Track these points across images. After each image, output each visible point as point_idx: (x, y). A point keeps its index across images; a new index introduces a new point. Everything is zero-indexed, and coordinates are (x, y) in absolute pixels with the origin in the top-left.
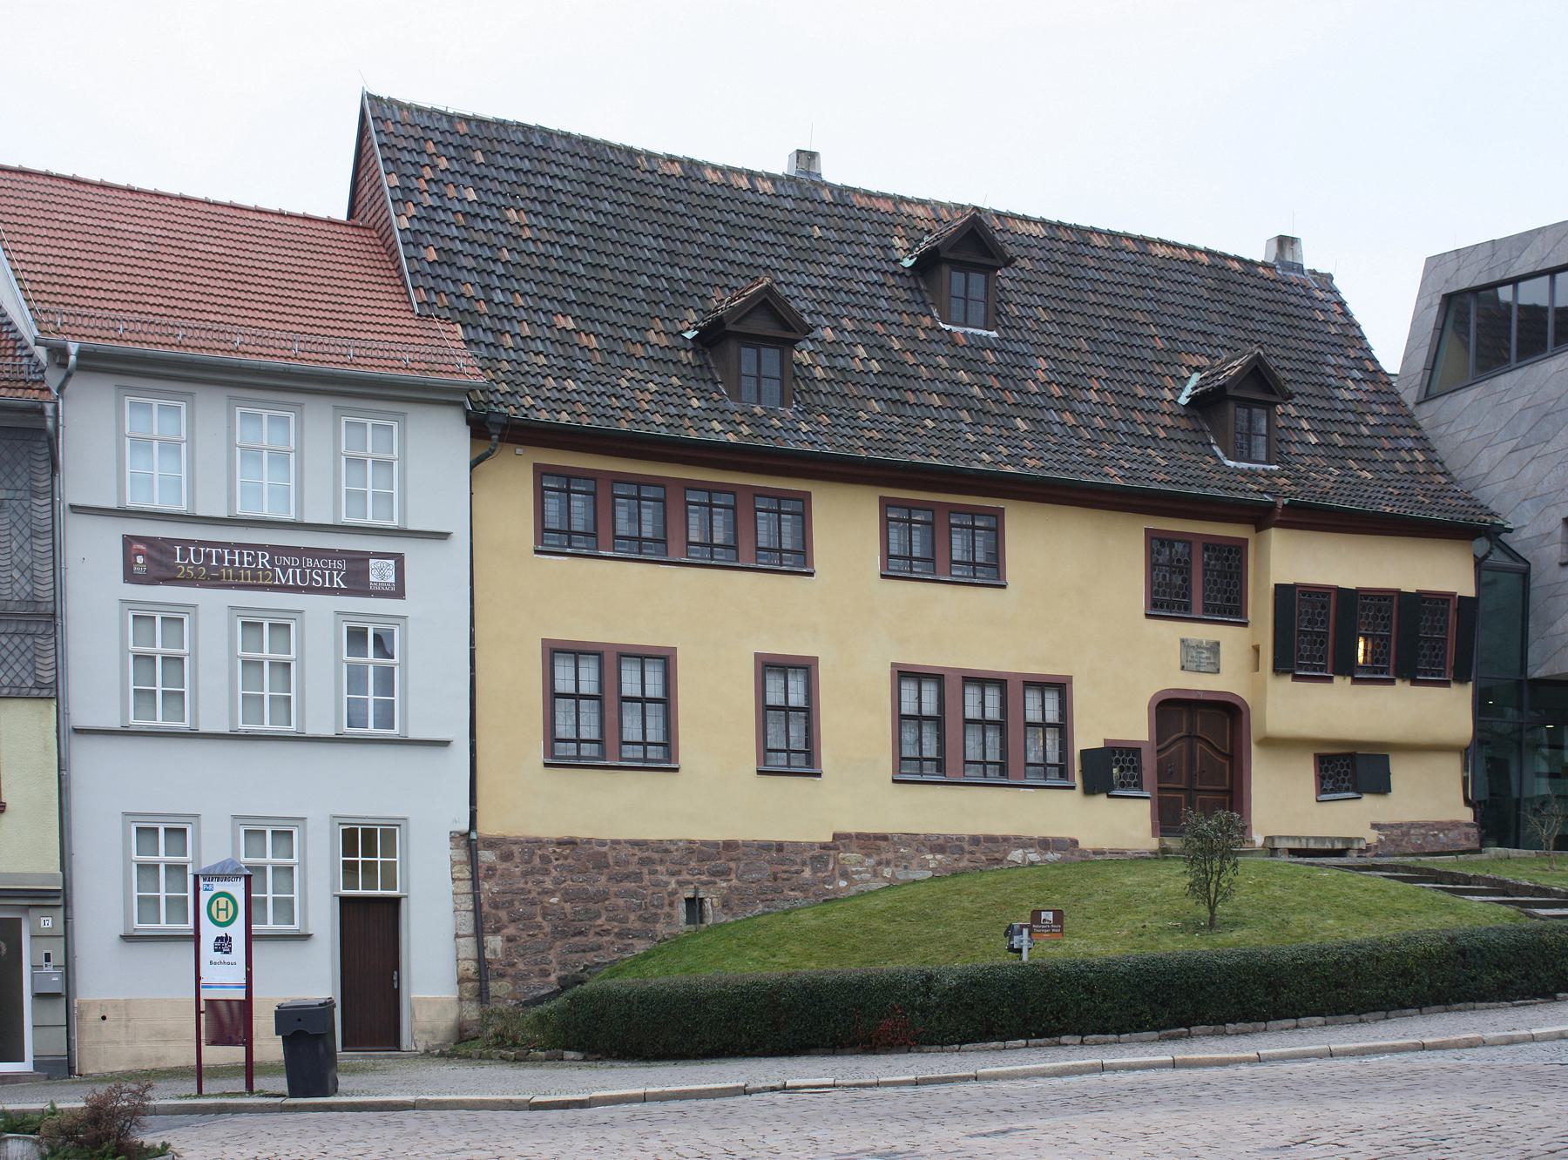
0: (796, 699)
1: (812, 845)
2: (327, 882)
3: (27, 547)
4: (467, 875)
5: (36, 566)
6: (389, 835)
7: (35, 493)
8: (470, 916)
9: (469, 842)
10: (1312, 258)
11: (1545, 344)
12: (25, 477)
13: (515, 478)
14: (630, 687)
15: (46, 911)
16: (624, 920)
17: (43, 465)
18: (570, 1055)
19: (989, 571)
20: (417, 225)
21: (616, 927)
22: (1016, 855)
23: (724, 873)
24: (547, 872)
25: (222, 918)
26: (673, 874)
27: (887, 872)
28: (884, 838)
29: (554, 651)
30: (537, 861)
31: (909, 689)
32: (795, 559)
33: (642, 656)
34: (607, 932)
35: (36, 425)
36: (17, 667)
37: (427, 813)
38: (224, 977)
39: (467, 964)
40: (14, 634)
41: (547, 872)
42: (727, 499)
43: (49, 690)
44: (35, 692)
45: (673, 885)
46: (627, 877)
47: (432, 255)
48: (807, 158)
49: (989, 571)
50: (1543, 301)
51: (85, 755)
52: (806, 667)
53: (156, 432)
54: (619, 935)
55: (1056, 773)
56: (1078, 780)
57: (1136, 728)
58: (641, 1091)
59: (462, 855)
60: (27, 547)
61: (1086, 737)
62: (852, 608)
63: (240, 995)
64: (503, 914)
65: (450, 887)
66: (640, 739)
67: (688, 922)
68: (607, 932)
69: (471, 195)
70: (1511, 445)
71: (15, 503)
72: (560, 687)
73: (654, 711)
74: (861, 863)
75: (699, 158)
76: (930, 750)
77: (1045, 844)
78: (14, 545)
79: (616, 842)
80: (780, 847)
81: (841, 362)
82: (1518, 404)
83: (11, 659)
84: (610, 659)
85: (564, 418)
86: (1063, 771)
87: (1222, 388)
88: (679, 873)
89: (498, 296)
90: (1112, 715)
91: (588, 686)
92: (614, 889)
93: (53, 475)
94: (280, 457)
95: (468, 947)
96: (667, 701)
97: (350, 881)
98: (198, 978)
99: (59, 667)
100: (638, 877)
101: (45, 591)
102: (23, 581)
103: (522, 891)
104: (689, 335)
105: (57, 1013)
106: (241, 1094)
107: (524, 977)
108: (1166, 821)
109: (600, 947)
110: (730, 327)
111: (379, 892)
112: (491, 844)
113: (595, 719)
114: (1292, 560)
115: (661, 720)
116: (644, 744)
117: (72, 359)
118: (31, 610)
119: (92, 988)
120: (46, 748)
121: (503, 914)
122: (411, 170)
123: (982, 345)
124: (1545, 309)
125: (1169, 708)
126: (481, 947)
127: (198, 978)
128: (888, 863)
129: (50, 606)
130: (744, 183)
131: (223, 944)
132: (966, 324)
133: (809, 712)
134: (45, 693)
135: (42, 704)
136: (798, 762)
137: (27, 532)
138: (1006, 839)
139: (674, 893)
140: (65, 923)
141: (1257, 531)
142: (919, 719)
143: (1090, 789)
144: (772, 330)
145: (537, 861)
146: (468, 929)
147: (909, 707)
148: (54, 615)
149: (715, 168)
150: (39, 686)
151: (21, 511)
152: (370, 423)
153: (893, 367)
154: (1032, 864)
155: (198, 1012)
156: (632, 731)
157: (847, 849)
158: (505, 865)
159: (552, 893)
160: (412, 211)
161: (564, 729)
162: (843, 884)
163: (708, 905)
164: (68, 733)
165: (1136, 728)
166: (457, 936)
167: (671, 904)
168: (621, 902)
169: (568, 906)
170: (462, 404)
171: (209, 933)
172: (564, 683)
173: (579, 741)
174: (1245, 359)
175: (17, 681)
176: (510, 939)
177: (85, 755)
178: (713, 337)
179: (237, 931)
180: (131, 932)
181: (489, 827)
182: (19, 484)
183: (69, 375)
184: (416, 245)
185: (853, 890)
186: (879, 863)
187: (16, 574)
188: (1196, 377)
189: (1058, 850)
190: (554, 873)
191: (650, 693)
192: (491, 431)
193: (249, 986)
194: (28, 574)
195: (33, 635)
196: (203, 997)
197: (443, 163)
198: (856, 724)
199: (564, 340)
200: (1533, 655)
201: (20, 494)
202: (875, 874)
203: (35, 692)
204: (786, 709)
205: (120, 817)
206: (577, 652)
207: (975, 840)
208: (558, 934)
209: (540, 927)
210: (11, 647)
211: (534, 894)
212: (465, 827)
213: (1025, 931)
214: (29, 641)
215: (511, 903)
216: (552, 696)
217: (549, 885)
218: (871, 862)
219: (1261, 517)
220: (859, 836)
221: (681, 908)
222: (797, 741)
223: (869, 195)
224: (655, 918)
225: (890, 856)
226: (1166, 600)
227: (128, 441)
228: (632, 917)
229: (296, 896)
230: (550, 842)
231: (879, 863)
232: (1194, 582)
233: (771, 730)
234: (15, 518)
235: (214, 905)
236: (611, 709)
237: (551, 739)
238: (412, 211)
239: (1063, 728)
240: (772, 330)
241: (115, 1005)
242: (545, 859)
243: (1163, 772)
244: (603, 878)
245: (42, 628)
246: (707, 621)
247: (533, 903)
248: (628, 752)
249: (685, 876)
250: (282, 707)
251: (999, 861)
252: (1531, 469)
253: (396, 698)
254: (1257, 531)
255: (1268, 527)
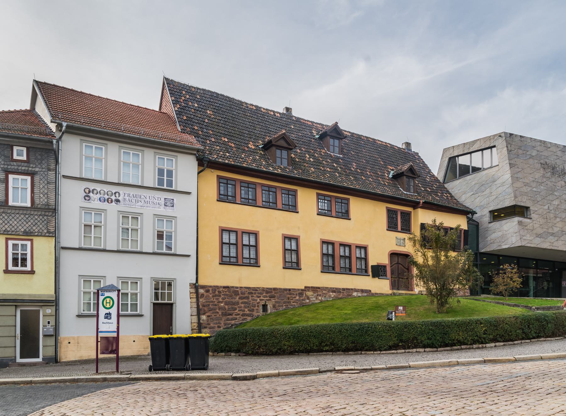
0: (294, 247)
1: (299, 290)
2: (149, 298)
3: (46, 187)
4: (195, 296)
5: (49, 193)
6: (170, 285)
7: (49, 170)
8: (195, 309)
9: (196, 287)
10: (414, 149)
11: (469, 173)
12: (46, 165)
13: (211, 177)
14: (246, 242)
15: (49, 307)
16: (244, 311)
17: (53, 161)
18: (233, 354)
19: (345, 215)
20: (180, 110)
21: (241, 313)
22: (355, 294)
23: (273, 297)
24: (220, 296)
25: (108, 306)
26: (259, 297)
27: (320, 298)
28: (319, 288)
29: (223, 230)
30: (217, 293)
31: (325, 246)
32: (293, 208)
33: (249, 233)
34: (239, 314)
35: (50, 148)
36: (41, 226)
37: (182, 275)
38: (108, 327)
39: (195, 324)
40: (40, 215)
41: (220, 296)
42: (274, 190)
43: (54, 234)
44: (47, 234)
45: (258, 300)
46: (244, 298)
47: (185, 118)
48: (288, 109)
49: (345, 215)
50: (468, 164)
51: (64, 255)
52: (297, 239)
53: (94, 155)
54: (242, 315)
55: (363, 272)
56: (370, 273)
57: (385, 260)
58: (277, 371)
59: (193, 290)
60: (46, 187)
61: (372, 261)
62: (309, 221)
63: (115, 335)
64: (206, 309)
65: (189, 300)
66: (248, 257)
67: (263, 312)
68: (239, 314)
69: (196, 105)
70: (472, 193)
71: (42, 173)
72: (224, 241)
73: (253, 250)
74: (312, 295)
75: (260, 106)
76: (331, 264)
77: (362, 291)
78: (41, 186)
79: (241, 287)
80: (290, 290)
81: (303, 158)
82: (474, 183)
83: (39, 223)
84: (240, 234)
85: (227, 161)
86: (366, 271)
87: (403, 172)
88: (260, 297)
89: (205, 130)
90: (378, 256)
91: (233, 241)
92: (241, 301)
93: (56, 165)
94: (136, 166)
95: (195, 319)
96: (256, 246)
97: (157, 298)
98: (98, 329)
99: (57, 228)
100: (248, 298)
101: (52, 202)
102: (44, 198)
103: (212, 302)
104: (260, 147)
105: (51, 341)
106: (113, 373)
107: (213, 328)
108: (394, 286)
109: (236, 319)
110: (273, 143)
111: (166, 301)
112: (203, 287)
113: (235, 251)
114: (423, 217)
115: (254, 252)
116: (250, 258)
117: (64, 128)
118: (47, 207)
119: (64, 333)
120: (50, 253)
121: (206, 309)
122: (178, 97)
123: (339, 158)
124: (469, 166)
125: (393, 255)
126: (199, 319)
127: (98, 329)
128: (320, 296)
129: (54, 207)
130: (272, 113)
131: (108, 316)
132: (334, 153)
133: (297, 251)
134: (51, 235)
135: (50, 239)
136: (295, 265)
137: (46, 182)
138: (352, 289)
139: (258, 303)
140: (56, 311)
141: (414, 209)
142: (328, 255)
143: (374, 276)
144: (285, 145)
145: (217, 293)
146: (195, 313)
147: (325, 251)
148: (55, 209)
149: (264, 109)
150: (49, 232)
151: (44, 175)
152: (166, 158)
153: (317, 160)
154: (359, 296)
155: (97, 342)
156: (246, 254)
157: (309, 291)
158: (208, 294)
159: (222, 302)
160: (179, 106)
161: (225, 253)
162: (308, 301)
163: (269, 307)
164: (59, 249)
165: (385, 260)
166: (191, 315)
167: (258, 306)
168: (243, 305)
169: (226, 307)
170: (195, 154)
171: (103, 312)
172: (226, 240)
173: (230, 257)
174: (408, 166)
175: (41, 231)
176: (208, 316)
177: (64, 255)
178: (268, 146)
179: (114, 311)
180: (80, 314)
181: (201, 282)
182: (44, 166)
183: (63, 133)
184: (180, 115)
185: (311, 303)
186: (318, 295)
187: (42, 196)
188: (392, 172)
189: (365, 293)
190: (222, 296)
191: (251, 244)
192: (205, 163)
193: (118, 332)
194: (46, 196)
195: (47, 216)
196: (356, 273)
197: (188, 97)
198: (311, 256)
199: (224, 143)
200: (481, 246)
201: (44, 170)
202: (317, 299)
203: (47, 234)
204: (291, 250)
205: (78, 277)
206: (229, 231)
207: (344, 289)
208: (224, 314)
209: (218, 313)
210: (39, 219)
211: (216, 303)
212: (194, 282)
213: (394, 313)
214: (45, 218)
215: (209, 305)
216: (222, 243)
217: (221, 300)
218: (316, 294)
219: (415, 205)
220: (312, 287)
221: (261, 308)
222: (294, 260)
223: (305, 120)
224: (253, 310)
225: (321, 293)
226: (392, 226)
227: (84, 157)
228: (246, 310)
229: (138, 302)
230: (221, 287)
231: (318, 295)
232: (398, 222)
233: (287, 256)
234: (42, 177)
235: (111, 305)
236: (239, 249)
237: (222, 256)
238: (179, 106)
239: (366, 259)
240: (285, 145)
241: (74, 338)
242: (219, 292)
243: (392, 273)
244: (237, 298)
245: (51, 213)
246: (268, 225)
247: (216, 305)
248: (245, 261)
249: (262, 298)
250: (134, 296)
251: (350, 295)
252: (478, 199)
253: (173, 242)
254: (414, 209)
255: (418, 208)
